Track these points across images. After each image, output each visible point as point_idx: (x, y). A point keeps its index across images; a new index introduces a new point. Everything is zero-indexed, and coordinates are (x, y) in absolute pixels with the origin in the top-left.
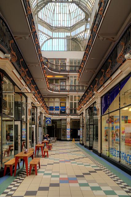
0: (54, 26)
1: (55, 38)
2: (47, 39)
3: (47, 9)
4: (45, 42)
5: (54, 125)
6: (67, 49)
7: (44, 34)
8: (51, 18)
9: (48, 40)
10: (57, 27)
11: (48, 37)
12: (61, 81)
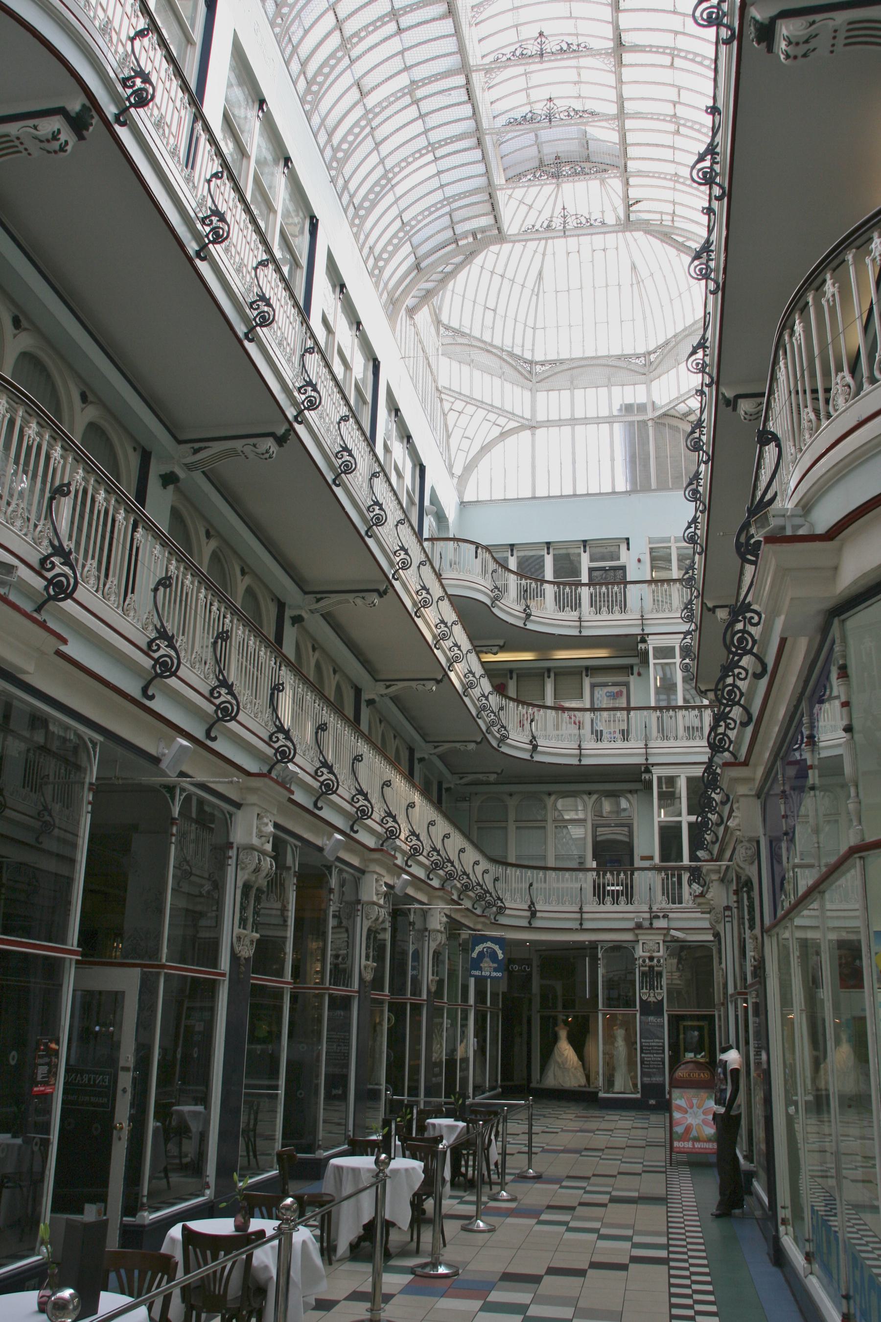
0: (539, 357)
1: (548, 423)
2: (496, 431)
3: (497, 279)
4: (485, 449)
5: (559, 987)
6: (633, 481)
7: (480, 404)
8: (521, 318)
9: (504, 435)
10: (562, 362)
11: (502, 421)
12: (593, 686)
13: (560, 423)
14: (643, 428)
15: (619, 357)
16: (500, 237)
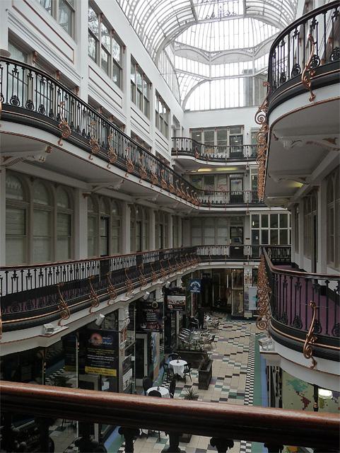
1: (215, 78)
2: (197, 82)
4: (193, 89)
9: (199, 84)
10: (221, 52)
11: (198, 79)
13: (219, 78)
14: (250, 77)
15: (242, 50)
16: (196, 22)
